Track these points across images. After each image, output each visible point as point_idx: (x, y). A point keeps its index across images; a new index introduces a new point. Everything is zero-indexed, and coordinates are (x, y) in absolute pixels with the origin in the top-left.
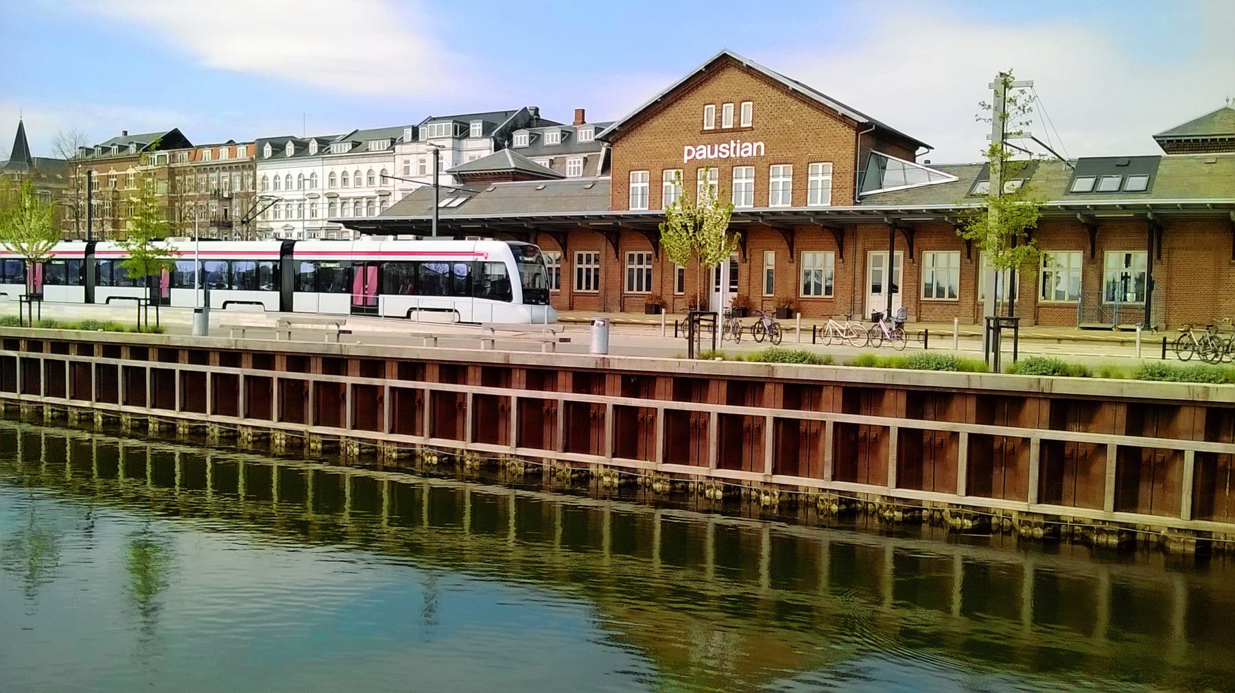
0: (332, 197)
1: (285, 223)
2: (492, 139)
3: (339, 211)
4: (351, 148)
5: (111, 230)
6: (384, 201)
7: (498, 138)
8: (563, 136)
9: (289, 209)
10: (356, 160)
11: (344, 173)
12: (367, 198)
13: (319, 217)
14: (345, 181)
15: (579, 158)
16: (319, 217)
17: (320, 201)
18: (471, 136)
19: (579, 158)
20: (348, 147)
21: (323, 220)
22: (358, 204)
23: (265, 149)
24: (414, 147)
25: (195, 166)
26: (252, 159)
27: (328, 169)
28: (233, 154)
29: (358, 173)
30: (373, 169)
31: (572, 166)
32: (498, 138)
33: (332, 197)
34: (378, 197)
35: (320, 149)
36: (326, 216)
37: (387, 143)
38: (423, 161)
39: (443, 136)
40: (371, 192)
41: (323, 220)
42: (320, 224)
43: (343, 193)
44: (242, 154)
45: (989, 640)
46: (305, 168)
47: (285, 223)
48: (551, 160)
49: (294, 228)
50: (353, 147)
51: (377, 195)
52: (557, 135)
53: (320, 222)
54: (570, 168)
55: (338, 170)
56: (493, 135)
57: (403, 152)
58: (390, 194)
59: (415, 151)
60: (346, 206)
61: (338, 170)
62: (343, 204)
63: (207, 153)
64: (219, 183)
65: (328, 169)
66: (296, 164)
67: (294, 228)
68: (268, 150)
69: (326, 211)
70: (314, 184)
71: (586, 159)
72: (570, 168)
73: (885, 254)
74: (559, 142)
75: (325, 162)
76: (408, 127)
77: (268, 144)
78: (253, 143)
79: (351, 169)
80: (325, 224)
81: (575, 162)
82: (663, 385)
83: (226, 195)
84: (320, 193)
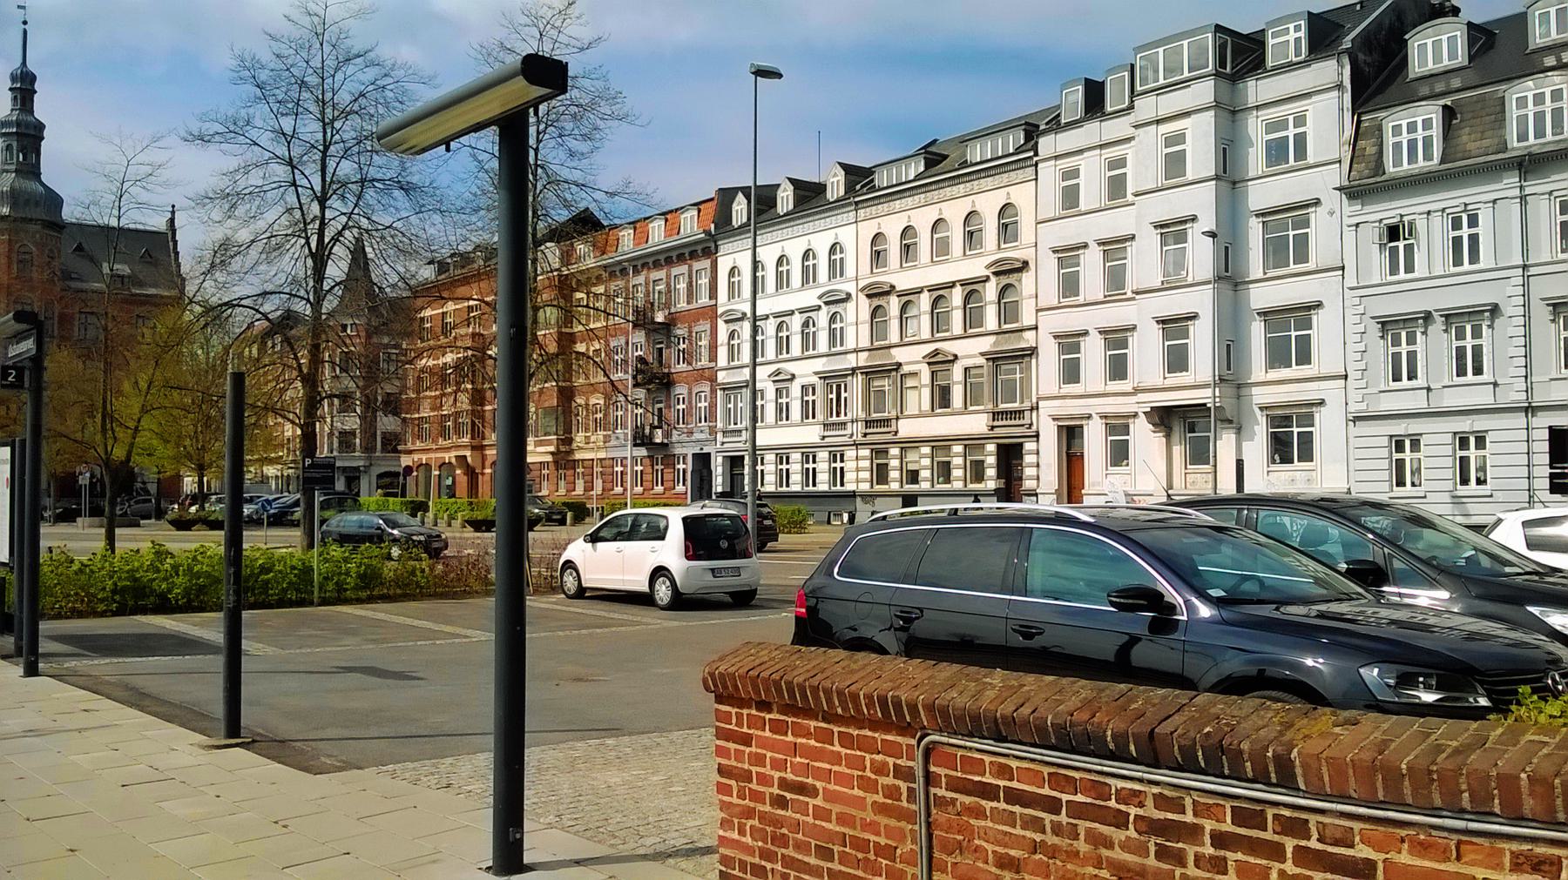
0: (877, 293)
1: (931, 347)
2: (1346, 60)
3: (894, 325)
4: (922, 169)
5: (470, 408)
6: (879, 307)
7: (1361, 57)
8: (1471, 42)
9: (784, 334)
10: (935, 195)
11: (907, 231)
12: (964, 283)
13: (850, 343)
14: (908, 250)
15: (1431, 112)
16: (850, 343)
17: (851, 306)
18: (1270, 63)
19: (1431, 112)
20: (917, 167)
21: (856, 351)
22: (942, 303)
23: (735, 207)
24: (1093, 131)
25: (605, 267)
26: (707, 232)
27: (868, 230)
28: (673, 229)
29: (941, 226)
30: (977, 208)
31: (1405, 138)
32: (1361, 57)
33: (877, 293)
34: (993, 279)
35: (850, 189)
36: (865, 342)
37: (1016, 138)
38: (1073, 173)
39: (1186, 74)
40: (975, 267)
41: (856, 351)
42: (851, 361)
43: (903, 281)
44: (691, 226)
45: (469, 632)
46: (817, 236)
47: (931, 347)
48: (1445, 107)
49: (793, 377)
50: (927, 167)
51: (987, 273)
52: (1452, 40)
53: (852, 357)
54: (1397, 146)
55: (892, 227)
56: (1347, 43)
57: (1061, 149)
58: (1026, 263)
59: (1096, 141)
60: (911, 312)
61: (892, 227)
62: (904, 308)
63: (627, 237)
64: (647, 294)
65: (868, 230)
66: (799, 229)
67: (793, 377)
68: (740, 209)
69: (865, 330)
70: (836, 269)
71: (1449, 113)
72: (1397, 146)
73: (1255, 390)
74: (1462, 58)
75: (861, 212)
76: (1073, 83)
77: (740, 197)
78: (712, 199)
79: (923, 220)
80: (863, 359)
81: (1412, 128)
82: (1226, 664)
83: (660, 317)
84: (850, 287)
